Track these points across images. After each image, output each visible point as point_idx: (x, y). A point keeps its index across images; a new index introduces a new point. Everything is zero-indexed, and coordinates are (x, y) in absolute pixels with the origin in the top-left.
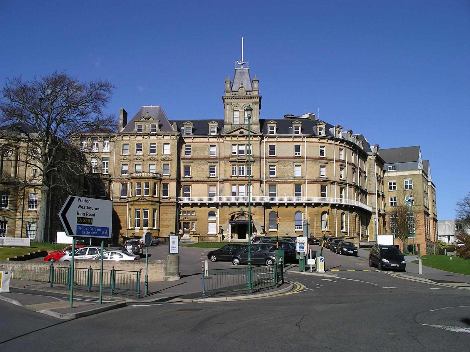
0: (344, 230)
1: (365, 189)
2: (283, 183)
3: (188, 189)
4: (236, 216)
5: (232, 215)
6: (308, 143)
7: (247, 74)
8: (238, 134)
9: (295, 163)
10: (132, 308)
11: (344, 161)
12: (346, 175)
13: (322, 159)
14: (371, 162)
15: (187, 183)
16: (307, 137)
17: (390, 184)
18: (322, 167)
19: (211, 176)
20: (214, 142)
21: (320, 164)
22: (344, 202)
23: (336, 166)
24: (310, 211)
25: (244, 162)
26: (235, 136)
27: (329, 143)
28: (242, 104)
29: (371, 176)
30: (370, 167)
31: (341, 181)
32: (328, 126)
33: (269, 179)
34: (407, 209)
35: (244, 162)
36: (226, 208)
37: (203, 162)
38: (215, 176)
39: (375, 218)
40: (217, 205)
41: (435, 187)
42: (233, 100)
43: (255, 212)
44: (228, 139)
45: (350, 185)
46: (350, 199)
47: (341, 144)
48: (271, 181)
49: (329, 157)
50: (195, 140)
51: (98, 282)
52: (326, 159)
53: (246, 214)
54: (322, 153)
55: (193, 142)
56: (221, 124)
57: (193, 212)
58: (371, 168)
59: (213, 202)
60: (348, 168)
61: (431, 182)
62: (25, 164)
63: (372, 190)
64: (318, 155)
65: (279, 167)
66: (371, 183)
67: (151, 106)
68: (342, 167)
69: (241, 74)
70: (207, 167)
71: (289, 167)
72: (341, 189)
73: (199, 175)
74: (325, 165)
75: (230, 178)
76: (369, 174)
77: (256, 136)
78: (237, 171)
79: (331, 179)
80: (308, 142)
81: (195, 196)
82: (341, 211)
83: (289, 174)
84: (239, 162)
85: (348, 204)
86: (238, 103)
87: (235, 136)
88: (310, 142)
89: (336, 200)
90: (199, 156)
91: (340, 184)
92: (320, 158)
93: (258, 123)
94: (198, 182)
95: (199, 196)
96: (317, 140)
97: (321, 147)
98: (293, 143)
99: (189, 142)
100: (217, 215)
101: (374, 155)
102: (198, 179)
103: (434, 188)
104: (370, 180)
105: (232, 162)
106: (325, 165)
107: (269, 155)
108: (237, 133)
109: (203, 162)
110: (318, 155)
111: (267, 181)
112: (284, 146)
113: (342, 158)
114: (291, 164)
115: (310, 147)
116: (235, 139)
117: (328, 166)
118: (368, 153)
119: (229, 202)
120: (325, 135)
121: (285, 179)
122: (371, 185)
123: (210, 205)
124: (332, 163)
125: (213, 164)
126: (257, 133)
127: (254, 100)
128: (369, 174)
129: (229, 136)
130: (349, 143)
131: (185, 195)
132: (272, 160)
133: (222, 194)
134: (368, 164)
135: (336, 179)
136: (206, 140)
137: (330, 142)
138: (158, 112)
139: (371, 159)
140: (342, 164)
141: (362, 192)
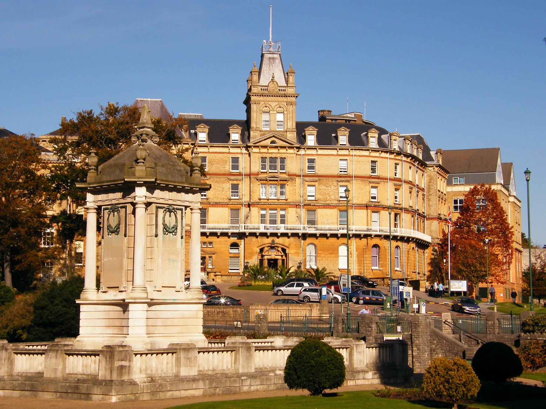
1: (423, 213)
2: (324, 208)
4: (266, 249)
5: (260, 247)
6: (356, 157)
7: (278, 61)
8: (269, 144)
9: (339, 183)
13: (373, 178)
14: (432, 175)
16: (355, 150)
17: (456, 202)
18: (372, 187)
19: (232, 198)
20: (237, 153)
21: (371, 185)
22: (400, 232)
23: (390, 186)
24: (358, 244)
25: (277, 180)
26: (265, 147)
27: (382, 158)
28: (273, 104)
29: (430, 195)
30: (430, 182)
31: (397, 206)
32: (382, 131)
33: (307, 202)
35: (277, 180)
36: (254, 239)
37: (223, 179)
38: (238, 198)
40: (241, 236)
41: (520, 201)
42: (261, 98)
43: (290, 245)
47: (398, 158)
48: (309, 205)
50: (212, 150)
52: (378, 178)
53: (278, 247)
55: (209, 152)
56: (246, 126)
57: (211, 243)
58: (431, 184)
59: (237, 231)
61: (514, 196)
62: (509, 316)
63: (432, 214)
64: (369, 173)
65: (320, 188)
66: (431, 203)
67: (149, 99)
68: (397, 187)
69: (271, 61)
70: (228, 186)
71: (333, 187)
73: (217, 196)
74: (376, 185)
75: (259, 201)
76: (429, 191)
77: (293, 148)
80: (357, 156)
81: (212, 222)
83: (333, 197)
84: (270, 180)
85: (403, 235)
86: (269, 103)
87: (265, 147)
88: (359, 156)
91: (395, 210)
92: (370, 177)
93: (293, 130)
94: (216, 204)
95: (218, 222)
96: (367, 153)
97: (372, 162)
98: (337, 157)
99: (204, 153)
100: (242, 247)
101: (437, 167)
102: (216, 200)
103: (518, 203)
104: (429, 200)
105: (261, 180)
106: (376, 185)
107: (307, 171)
109: (223, 179)
110: (369, 173)
111: (305, 205)
112: (329, 161)
114: (335, 183)
115: (357, 162)
116: (265, 150)
117: (381, 186)
118: (427, 163)
120: (378, 147)
121: (327, 202)
123: (234, 235)
124: (386, 183)
125: (235, 182)
126: (293, 143)
127: (289, 99)
128: (429, 191)
129: (258, 147)
130: (407, 155)
133: (248, 221)
134: (428, 178)
136: (226, 150)
137: (383, 155)
138: (159, 109)
140: (398, 182)
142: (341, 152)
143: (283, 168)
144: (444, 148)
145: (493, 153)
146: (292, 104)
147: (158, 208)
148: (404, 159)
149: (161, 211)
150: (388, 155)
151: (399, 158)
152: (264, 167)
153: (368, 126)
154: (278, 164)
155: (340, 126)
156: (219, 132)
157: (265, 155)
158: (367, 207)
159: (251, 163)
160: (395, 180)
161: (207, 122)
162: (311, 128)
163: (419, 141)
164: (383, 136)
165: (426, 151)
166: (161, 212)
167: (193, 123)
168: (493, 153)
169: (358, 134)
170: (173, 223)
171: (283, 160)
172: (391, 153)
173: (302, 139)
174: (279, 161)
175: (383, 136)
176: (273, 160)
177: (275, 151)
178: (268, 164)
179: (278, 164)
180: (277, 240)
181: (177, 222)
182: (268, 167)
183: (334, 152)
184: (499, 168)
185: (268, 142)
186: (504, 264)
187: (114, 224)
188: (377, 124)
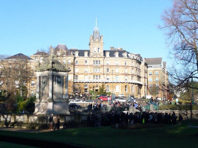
0: (133, 92)
3: (77, 76)
10: (23, 130)
11: (133, 67)
12: (134, 72)
15: (77, 74)
23: (130, 68)
32: (128, 53)
34: (96, 117)
39: (143, 86)
44: (92, 58)
45: (135, 75)
46: (135, 80)
49: (128, 65)
50: (80, 58)
51: (67, 118)
52: (127, 66)
54: (126, 64)
56: (89, 52)
60: (135, 69)
72: (132, 77)
78: (95, 71)
79: (129, 73)
82: (132, 85)
89: (131, 81)
90: (81, 64)
96: (124, 59)
108: (95, 56)
110: (125, 65)
113: (133, 66)
116: (95, 58)
119: (93, 82)
122: (142, 74)
125: (108, 68)
131: (76, 79)
132: (108, 66)
135: (130, 73)
139: (143, 64)
141: (139, 77)
142: (116, 59)
143: (99, 63)
144: (146, 58)
145: (161, 59)
146: (102, 45)
147: (56, 76)
148: (135, 61)
149: (57, 77)
150: (130, 60)
151: (133, 60)
152: (94, 63)
153: (124, 51)
154: (98, 62)
155: (116, 51)
156: (81, 53)
157: (94, 60)
158: (124, 74)
159: (90, 61)
160: (132, 67)
161: (78, 51)
162: (108, 52)
163: (139, 55)
164: (128, 54)
165: (141, 58)
166: (57, 77)
167: (74, 51)
168: (161, 59)
169: (121, 53)
170: (60, 80)
171: (99, 61)
172: (131, 59)
173: (105, 55)
174: (98, 61)
175: (128, 54)
176: (97, 61)
177: (98, 58)
178: (95, 62)
179: (98, 62)
180: (98, 84)
181: (61, 80)
182: (95, 63)
183: (115, 59)
184: (162, 63)
185: (95, 56)
186: (153, 115)
187: (44, 81)
188: (127, 51)
